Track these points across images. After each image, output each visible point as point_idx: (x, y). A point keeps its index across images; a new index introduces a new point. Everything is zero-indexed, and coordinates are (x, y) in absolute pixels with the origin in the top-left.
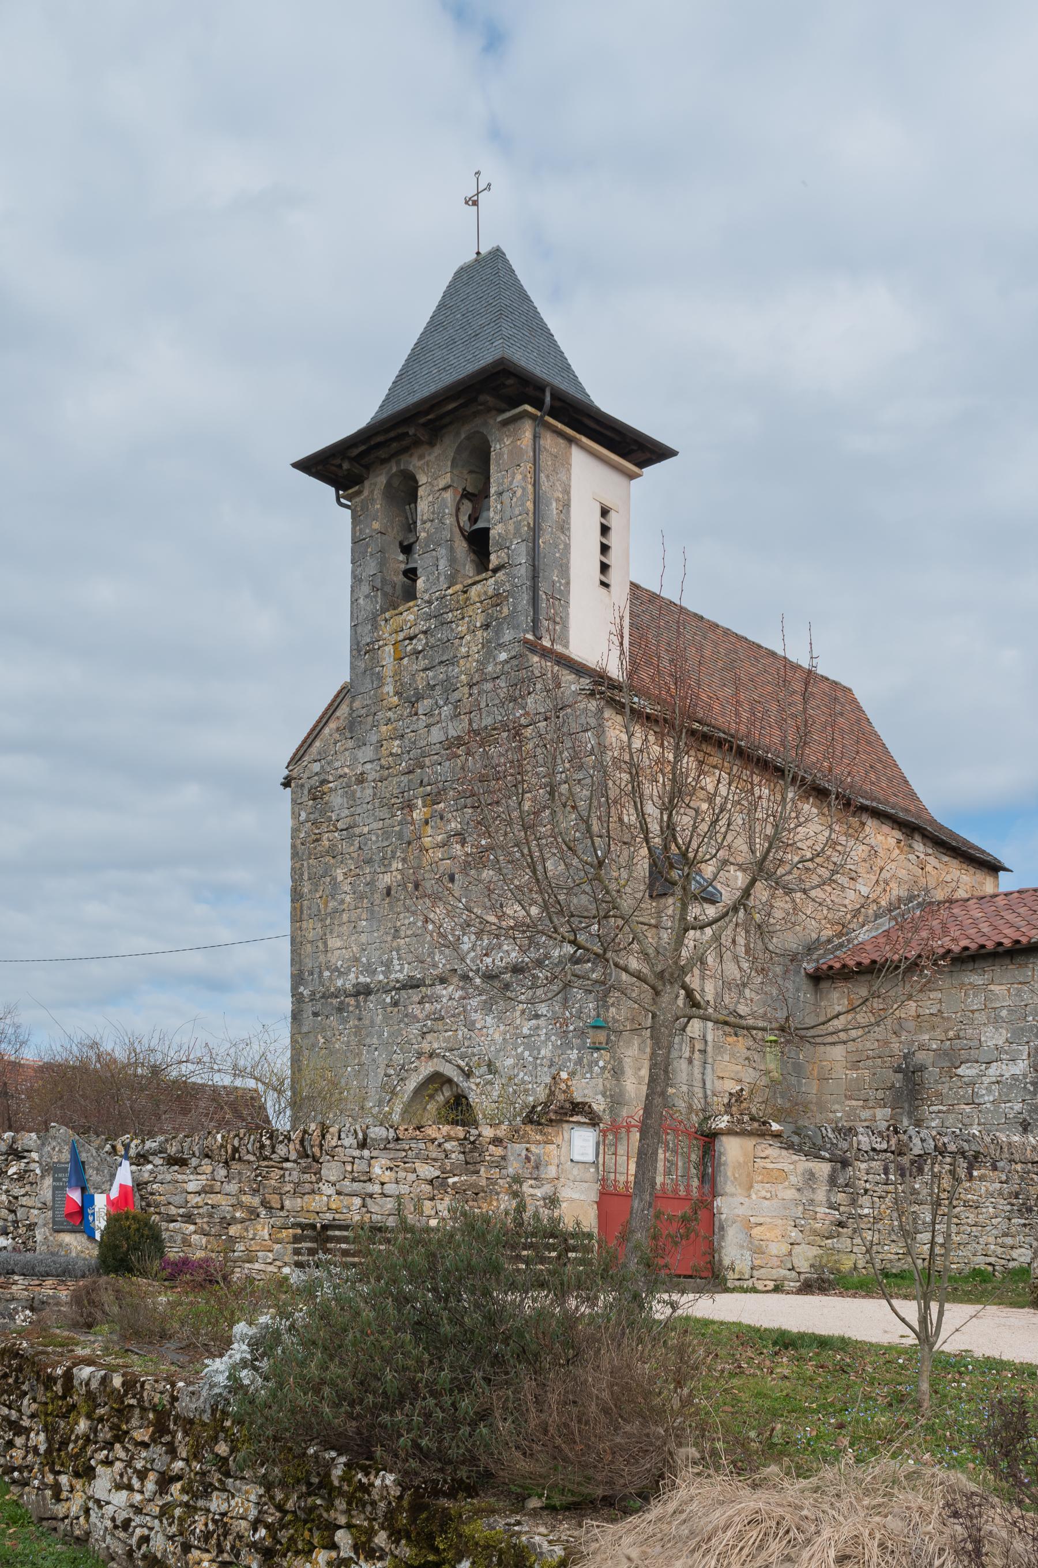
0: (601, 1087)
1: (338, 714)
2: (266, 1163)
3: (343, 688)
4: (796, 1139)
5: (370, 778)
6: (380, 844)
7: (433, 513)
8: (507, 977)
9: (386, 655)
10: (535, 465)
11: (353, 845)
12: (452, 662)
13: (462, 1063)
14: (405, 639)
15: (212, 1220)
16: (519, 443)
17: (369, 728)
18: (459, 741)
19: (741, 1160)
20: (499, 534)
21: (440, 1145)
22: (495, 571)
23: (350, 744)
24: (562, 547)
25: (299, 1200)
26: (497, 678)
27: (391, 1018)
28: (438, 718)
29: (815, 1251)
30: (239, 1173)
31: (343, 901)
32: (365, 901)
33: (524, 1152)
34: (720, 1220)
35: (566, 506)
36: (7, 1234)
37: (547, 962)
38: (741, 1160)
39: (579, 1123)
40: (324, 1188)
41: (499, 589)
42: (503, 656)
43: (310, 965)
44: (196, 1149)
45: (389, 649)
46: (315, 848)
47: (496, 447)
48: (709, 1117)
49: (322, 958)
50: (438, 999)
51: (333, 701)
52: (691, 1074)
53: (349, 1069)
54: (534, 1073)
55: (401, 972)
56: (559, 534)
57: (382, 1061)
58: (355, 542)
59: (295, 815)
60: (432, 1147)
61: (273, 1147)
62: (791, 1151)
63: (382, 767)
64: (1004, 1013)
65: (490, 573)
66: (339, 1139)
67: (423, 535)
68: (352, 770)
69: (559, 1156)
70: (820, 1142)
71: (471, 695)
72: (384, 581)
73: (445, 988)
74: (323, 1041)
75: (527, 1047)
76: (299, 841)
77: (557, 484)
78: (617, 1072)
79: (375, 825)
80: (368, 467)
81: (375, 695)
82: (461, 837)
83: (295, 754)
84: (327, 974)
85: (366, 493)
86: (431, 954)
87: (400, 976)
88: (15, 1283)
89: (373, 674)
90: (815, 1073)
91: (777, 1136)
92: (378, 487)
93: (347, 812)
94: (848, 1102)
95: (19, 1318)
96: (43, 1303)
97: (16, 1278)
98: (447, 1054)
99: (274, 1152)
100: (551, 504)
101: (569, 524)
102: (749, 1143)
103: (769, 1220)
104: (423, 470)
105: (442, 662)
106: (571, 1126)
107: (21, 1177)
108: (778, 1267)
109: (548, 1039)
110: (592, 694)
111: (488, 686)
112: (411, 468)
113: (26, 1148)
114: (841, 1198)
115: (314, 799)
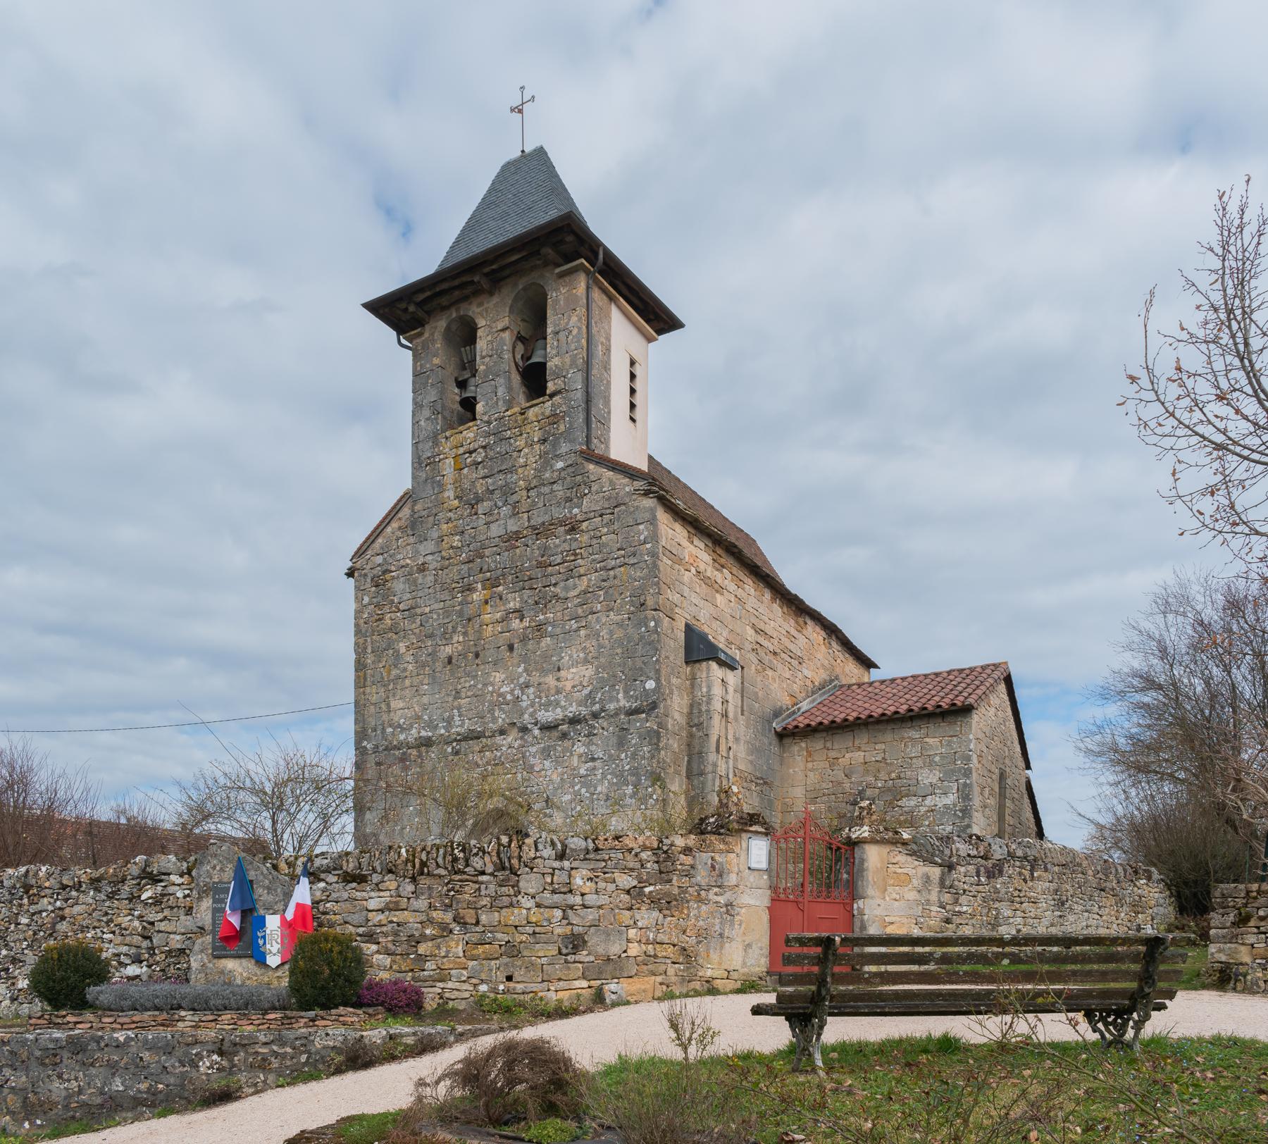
1: (400, 515)
2: (458, 877)
3: (406, 494)
5: (431, 567)
8: (564, 727)
12: (512, 470)
15: (398, 939)
18: (517, 536)
21: (636, 855)
22: (552, 396)
23: (412, 540)
25: (496, 914)
30: (429, 888)
31: (405, 670)
33: (710, 861)
35: (608, 350)
36: (141, 962)
39: (757, 832)
40: (523, 901)
42: (560, 465)
44: (377, 864)
45: (450, 461)
47: (552, 295)
49: (385, 717)
58: (416, 375)
59: (358, 599)
60: (629, 857)
61: (467, 861)
63: (443, 558)
64: (937, 759)
66: (537, 850)
67: (482, 368)
72: (443, 406)
75: (584, 785)
79: (436, 606)
80: (429, 313)
82: (520, 613)
84: (390, 730)
85: (426, 335)
86: (491, 711)
88: (182, 1019)
95: (204, 1066)
96: (235, 1045)
97: (183, 1013)
99: (467, 865)
107: (157, 901)
110: (646, 493)
111: (546, 490)
112: (470, 313)
113: (163, 870)
114: (947, 898)
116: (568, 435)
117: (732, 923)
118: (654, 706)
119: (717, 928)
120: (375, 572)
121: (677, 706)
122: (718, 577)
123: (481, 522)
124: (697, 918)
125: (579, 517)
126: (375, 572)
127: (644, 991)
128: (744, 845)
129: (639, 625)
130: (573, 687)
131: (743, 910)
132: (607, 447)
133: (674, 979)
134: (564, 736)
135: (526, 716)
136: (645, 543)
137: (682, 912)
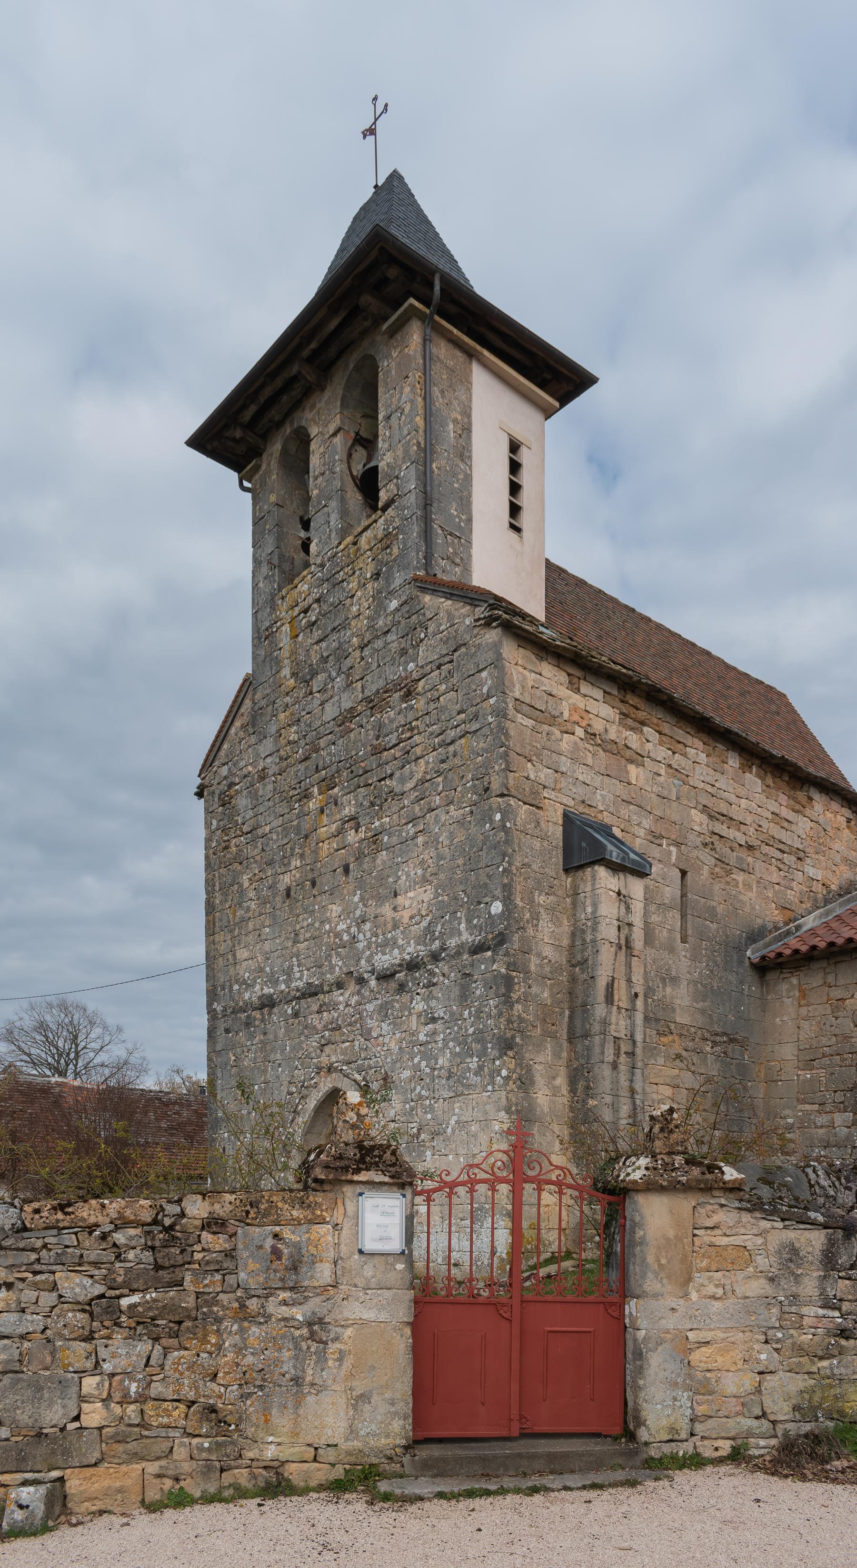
0: (504, 1102)
1: (242, 710)
3: (245, 681)
4: (765, 1192)
5: (271, 772)
6: (281, 843)
7: (324, 465)
9: (283, 636)
10: (425, 374)
11: (256, 847)
12: (344, 626)
13: (358, 1077)
14: (299, 614)
16: (406, 350)
17: (268, 718)
18: (351, 714)
19: (671, 1234)
20: (388, 465)
22: (384, 509)
23: (253, 739)
24: (461, 476)
26: (387, 632)
27: (293, 1030)
28: (330, 693)
29: (801, 1382)
31: (248, 909)
32: (268, 906)
33: (269, 1242)
34: (635, 1340)
37: (443, 955)
38: (671, 1234)
39: (370, 1183)
41: (388, 528)
42: (394, 604)
43: (222, 980)
45: (286, 628)
46: (224, 857)
48: (616, 1160)
50: (334, 1006)
51: (237, 697)
52: (616, 1082)
53: (256, 1087)
54: (431, 1087)
55: (301, 979)
56: (457, 461)
57: (285, 1078)
59: (208, 825)
62: (758, 1215)
65: (379, 512)
68: (255, 767)
69: (337, 1245)
70: (805, 1195)
71: (362, 658)
72: (281, 557)
73: (342, 994)
74: (233, 1058)
75: (425, 1056)
76: (211, 851)
77: (455, 403)
78: (525, 1083)
81: (274, 682)
83: (206, 761)
85: (264, 467)
86: (328, 957)
87: (300, 984)
89: (271, 660)
90: (762, 1075)
91: (733, 1189)
92: (274, 456)
93: (251, 813)
94: (800, 1107)
98: (345, 1068)
100: (448, 425)
101: (470, 452)
102: (685, 1204)
103: (721, 1335)
104: (315, 421)
105: (334, 629)
106: (358, 1189)
108: (738, 1414)
109: (446, 1045)
110: (488, 622)
111: (379, 644)
115: (223, 805)
116: (401, 562)
117: (321, 1358)
118: (501, 939)
119: (288, 1367)
120: (221, 787)
121: (547, 939)
122: (633, 740)
123: (317, 702)
124: (240, 1350)
125: (415, 676)
126: (221, 787)
127: (120, 1491)
128: (350, 1207)
129: (481, 822)
130: (411, 918)
131: (349, 1332)
132: (467, 570)
133: (187, 1467)
134: (402, 988)
135: (363, 962)
136: (489, 697)
137: (204, 1340)
